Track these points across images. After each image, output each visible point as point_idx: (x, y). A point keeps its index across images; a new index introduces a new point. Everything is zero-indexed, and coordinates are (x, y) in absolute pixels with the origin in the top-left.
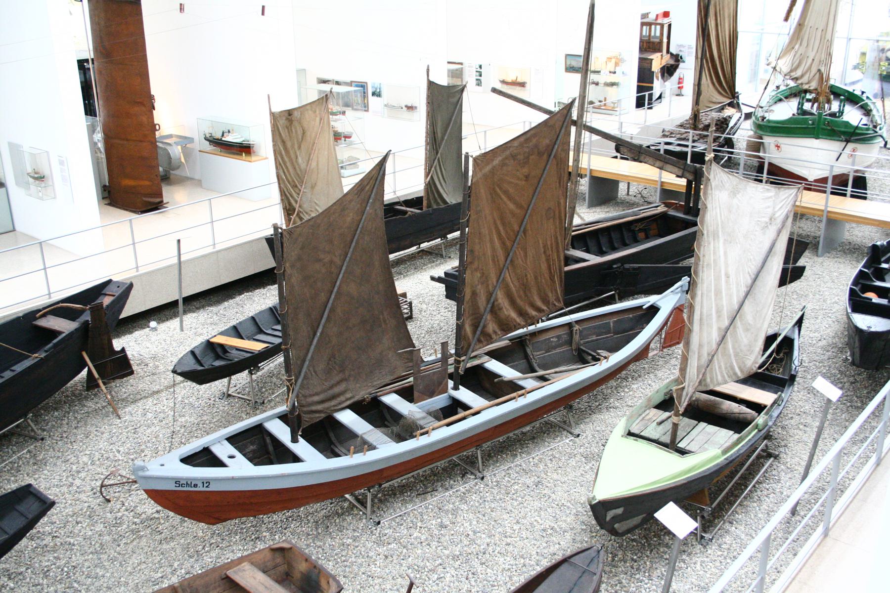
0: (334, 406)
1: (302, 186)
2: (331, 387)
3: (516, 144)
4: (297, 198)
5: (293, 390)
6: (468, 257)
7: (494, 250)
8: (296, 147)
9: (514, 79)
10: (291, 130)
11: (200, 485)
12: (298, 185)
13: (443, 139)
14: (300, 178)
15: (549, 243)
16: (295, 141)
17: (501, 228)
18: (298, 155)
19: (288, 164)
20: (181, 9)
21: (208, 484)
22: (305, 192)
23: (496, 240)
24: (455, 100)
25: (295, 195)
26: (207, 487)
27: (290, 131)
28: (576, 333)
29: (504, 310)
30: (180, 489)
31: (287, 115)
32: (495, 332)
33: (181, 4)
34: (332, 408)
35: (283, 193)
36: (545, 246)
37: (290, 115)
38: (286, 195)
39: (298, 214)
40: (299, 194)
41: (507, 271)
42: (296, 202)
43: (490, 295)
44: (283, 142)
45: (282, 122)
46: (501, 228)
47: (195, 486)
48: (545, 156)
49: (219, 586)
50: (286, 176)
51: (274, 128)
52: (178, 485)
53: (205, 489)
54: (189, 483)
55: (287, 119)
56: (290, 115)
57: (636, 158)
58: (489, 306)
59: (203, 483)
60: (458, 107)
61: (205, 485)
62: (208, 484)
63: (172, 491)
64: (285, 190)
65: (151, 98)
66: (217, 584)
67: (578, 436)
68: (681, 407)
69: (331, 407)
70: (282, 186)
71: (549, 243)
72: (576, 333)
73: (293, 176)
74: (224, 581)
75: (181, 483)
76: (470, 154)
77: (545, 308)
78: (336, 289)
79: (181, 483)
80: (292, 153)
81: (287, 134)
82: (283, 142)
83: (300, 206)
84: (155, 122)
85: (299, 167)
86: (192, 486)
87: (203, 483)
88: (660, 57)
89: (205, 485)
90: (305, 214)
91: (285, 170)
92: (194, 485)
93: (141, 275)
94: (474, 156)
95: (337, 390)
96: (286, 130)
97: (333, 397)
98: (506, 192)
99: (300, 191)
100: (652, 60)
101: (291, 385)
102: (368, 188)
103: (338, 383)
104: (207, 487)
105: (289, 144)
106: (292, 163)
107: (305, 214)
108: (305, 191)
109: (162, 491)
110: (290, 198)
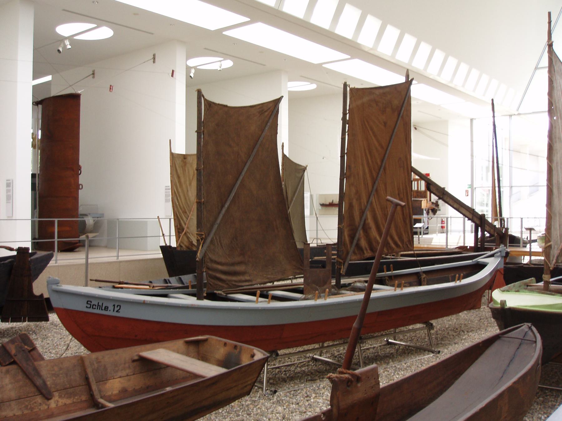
0: (235, 281)
1: (190, 213)
2: (233, 264)
3: (377, 92)
4: (186, 221)
5: (203, 243)
6: (347, 171)
7: (364, 173)
8: (188, 183)
9: (331, 201)
10: (185, 169)
11: (111, 308)
12: (188, 213)
13: (292, 199)
14: (189, 206)
15: (401, 188)
16: (188, 179)
17: (369, 158)
18: (189, 190)
19: (181, 194)
20: (110, 89)
21: (119, 307)
22: (192, 219)
23: (366, 166)
24: (300, 175)
25: (185, 219)
26: (117, 311)
27: (184, 170)
28: (424, 280)
29: (372, 229)
30: (91, 310)
31: (182, 158)
32: (366, 250)
33: (111, 86)
34: (234, 283)
35: (176, 215)
36: (399, 189)
37: (185, 158)
38: (177, 217)
39: (185, 233)
40: (187, 219)
41: (373, 197)
42: (185, 224)
43: (362, 213)
44: (179, 177)
45: (178, 162)
46: (369, 158)
47: (106, 308)
48: (396, 113)
49: (129, 367)
50: (178, 202)
51: (173, 164)
52: (89, 306)
53: (115, 314)
54: (100, 304)
55: (182, 161)
56: (185, 158)
57: (441, 197)
58: (362, 223)
59: (114, 305)
60: (302, 181)
61: (116, 309)
62: (119, 307)
63: (82, 312)
64: (178, 213)
65: (79, 168)
66: (127, 365)
67: (439, 352)
68: (551, 264)
69: (232, 281)
70: (175, 209)
71: (401, 188)
72: (424, 280)
73: (184, 204)
74: (135, 363)
75: (92, 304)
76: (347, 83)
77: (401, 245)
78: (239, 182)
79: (92, 304)
80: (184, 186)
81: (182, 171)
82: (179, 177)
83: (188, 228)
84: (80, 183)
85: (189, 199)
86: (103, 308)
87: (114, 305)
88: (426, 201)
89: (116, 309)
90: (191, 235)
91: (179, 198)
92: (105, 307)
93: (58, 266)
94: (351, 87)
95: (238, 268)
96: (181, 169)
97: (235, 273)
98: (372, 129)
99: (189, 216)
100: (422, 201)
101: (202, 239)
102: (266, 113)
103: (240, 263)
104: (117, 311)
105: (182, 180)
106: (184, 195)
107: (191, 235)
108: (192, 217)
109: (72, 311)
110: (181, 220)
